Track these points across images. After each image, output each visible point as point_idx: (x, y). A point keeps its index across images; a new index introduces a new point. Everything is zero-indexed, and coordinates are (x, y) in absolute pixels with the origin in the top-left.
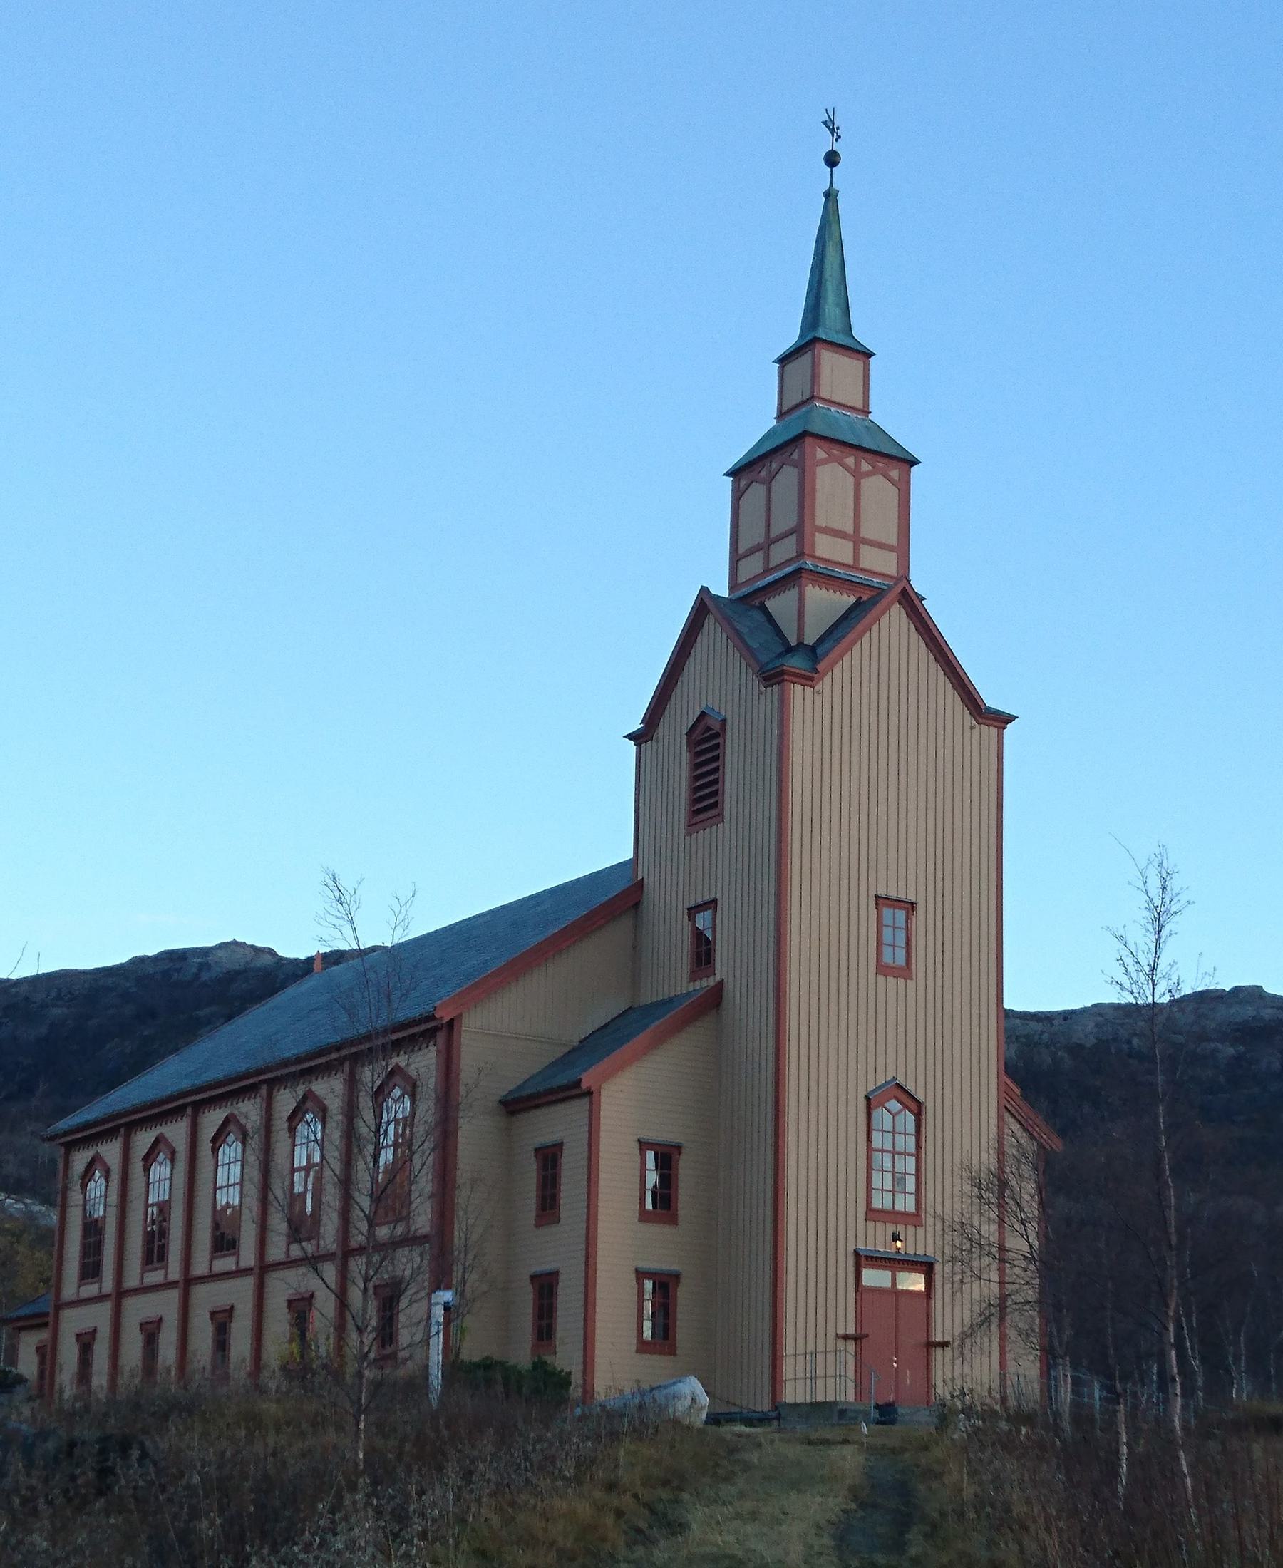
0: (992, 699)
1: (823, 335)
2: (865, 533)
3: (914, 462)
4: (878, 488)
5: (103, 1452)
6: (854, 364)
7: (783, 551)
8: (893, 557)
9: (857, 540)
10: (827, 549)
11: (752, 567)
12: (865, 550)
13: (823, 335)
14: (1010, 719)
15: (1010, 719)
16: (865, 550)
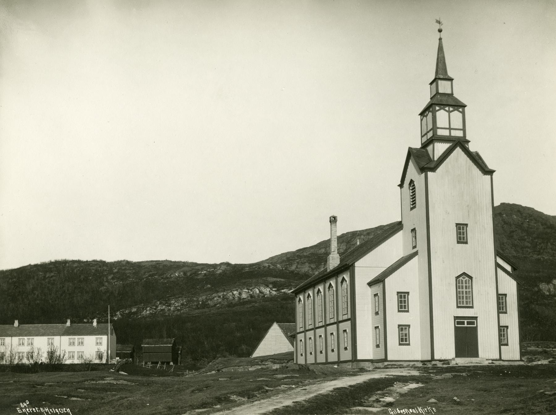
0: (491, 167)
1: (441, 73)
2: (452, 127)
3: (465, 106)
4: (456, 115)
5: (80, 288)
6: (449, 83)
7: (430, 135)
8: (462, 132)
9: (450, 129)
10: (440, 132)
11: (425, 139)
12: (452, 131)
13: (441, 73)
14: (494, 171)
15: (494, 171)
16: (452, 131)
